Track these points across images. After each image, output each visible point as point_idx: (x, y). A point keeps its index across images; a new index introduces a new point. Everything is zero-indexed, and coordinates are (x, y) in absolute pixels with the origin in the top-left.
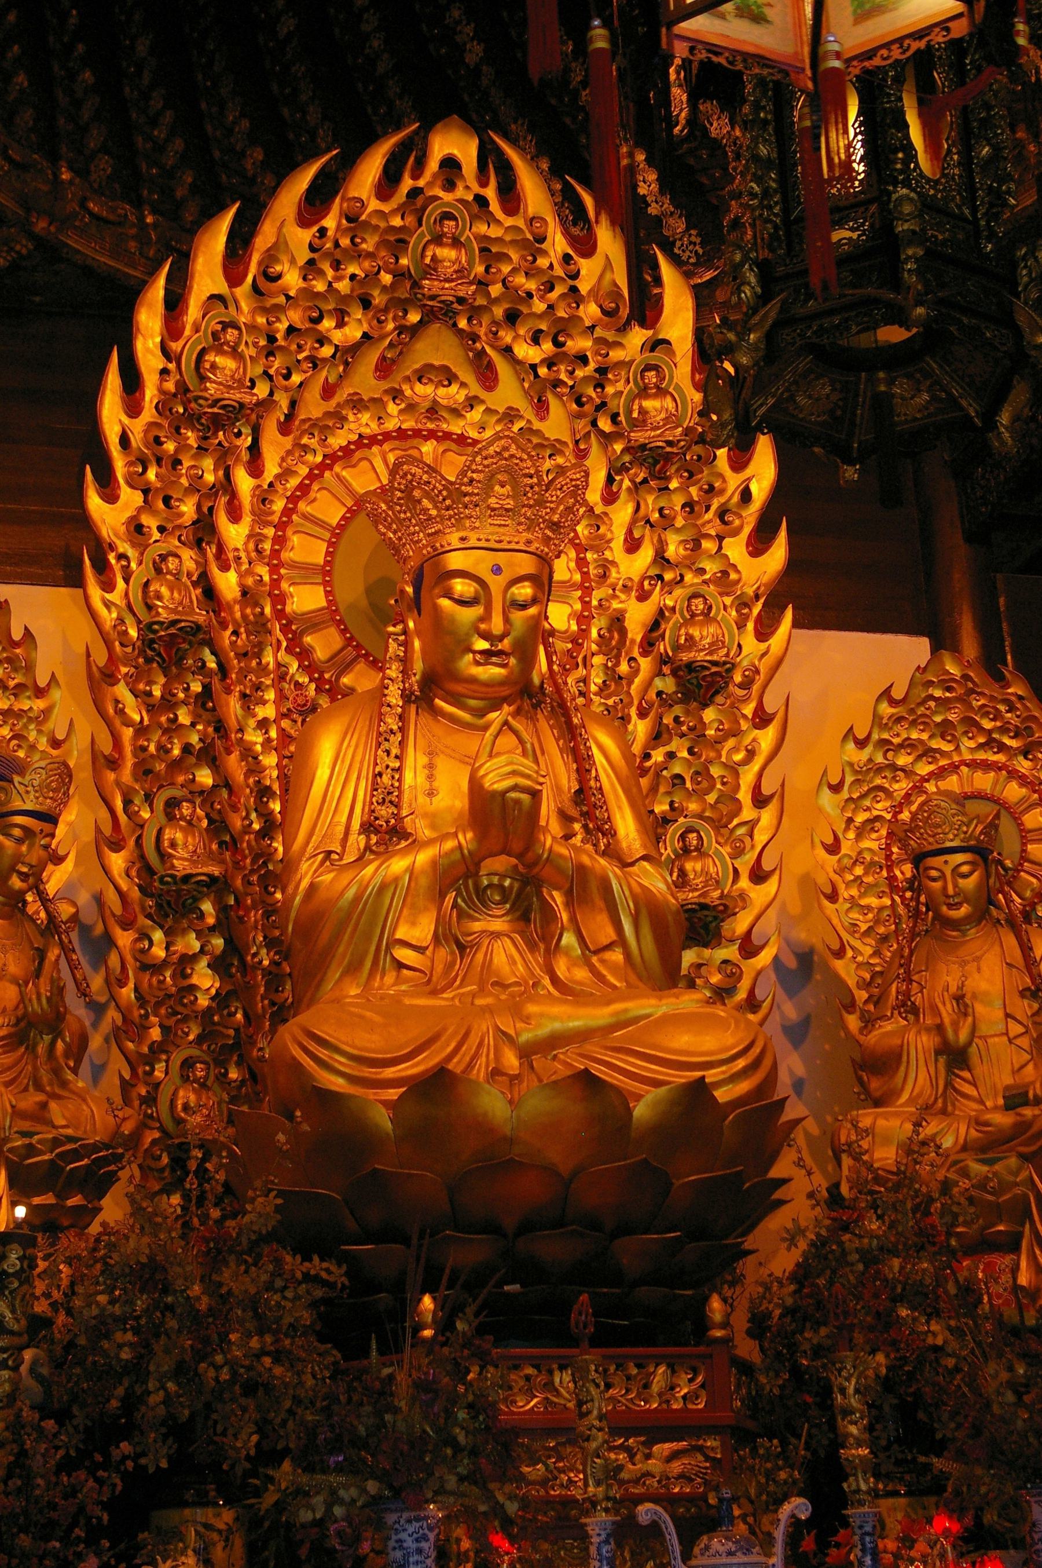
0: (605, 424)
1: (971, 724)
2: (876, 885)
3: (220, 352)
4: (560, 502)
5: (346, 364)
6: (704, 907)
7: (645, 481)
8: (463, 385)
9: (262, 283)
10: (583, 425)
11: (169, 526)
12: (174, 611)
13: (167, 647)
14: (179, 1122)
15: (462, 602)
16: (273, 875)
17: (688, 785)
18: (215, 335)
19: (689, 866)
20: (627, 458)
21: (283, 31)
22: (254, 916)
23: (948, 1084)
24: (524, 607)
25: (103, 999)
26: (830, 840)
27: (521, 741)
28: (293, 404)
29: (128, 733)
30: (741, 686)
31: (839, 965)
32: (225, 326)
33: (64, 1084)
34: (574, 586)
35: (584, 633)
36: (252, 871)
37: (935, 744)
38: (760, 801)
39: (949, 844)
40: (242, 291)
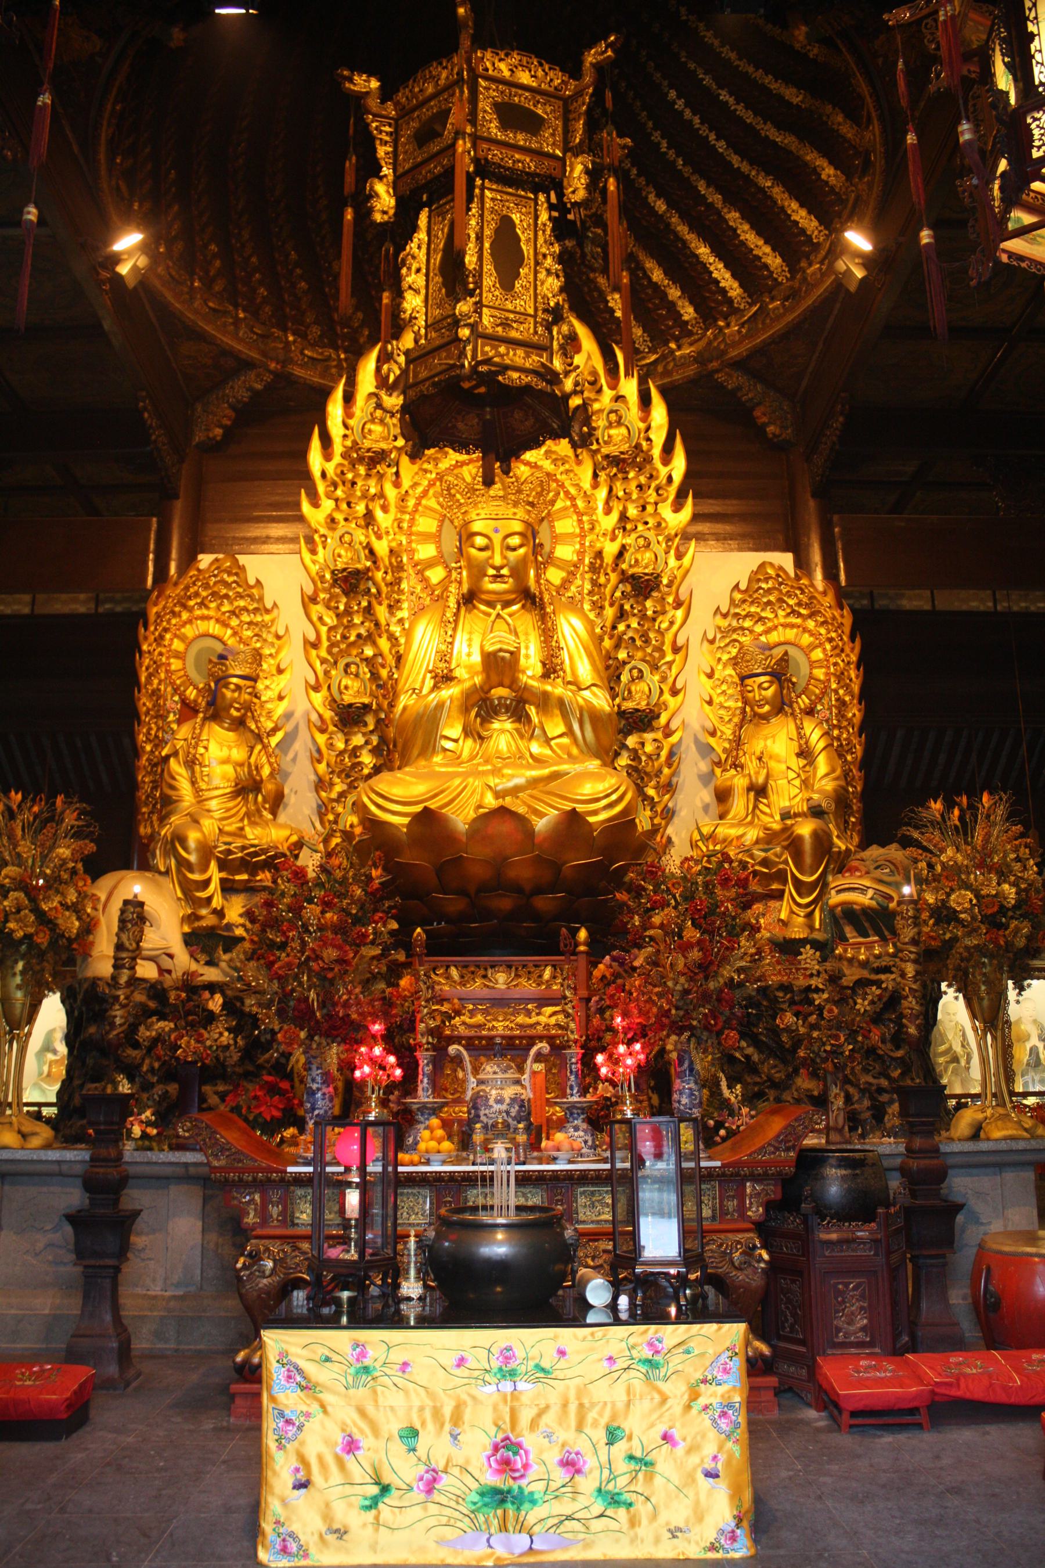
4: (531, 490)
6: (637, 710)
13: (350, 582)
15: (481, 549)
23: (755, 807)
24: (514, 549)
26: (709, 671)
29: (324, 630)
35: (581, 561)
37: (763, 614)
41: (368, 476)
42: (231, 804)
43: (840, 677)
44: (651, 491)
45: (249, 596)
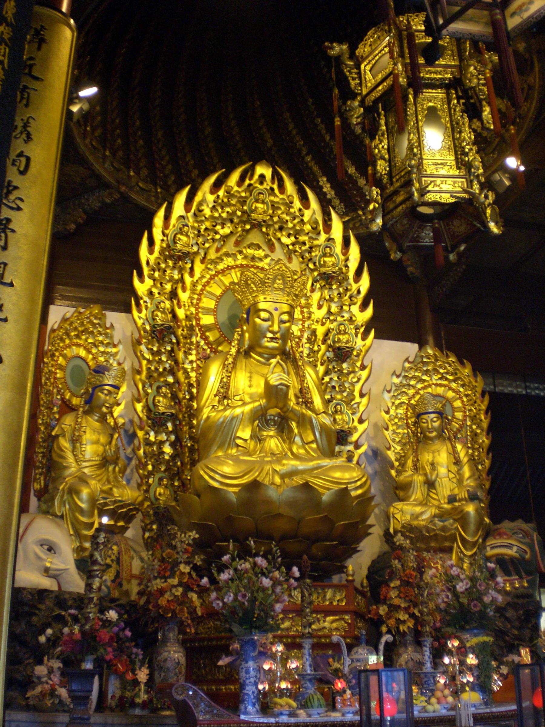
0: (311, 266)
1: (436, 371)
2: (402, 425)
3: (182, 234)
4: (299, 287)
5: (224, 241)
6: (342, 431)
7: (325, 285)
8: (264, 250)
9: (197, 213)
10: (304, 266)
11: (161, 293)
12: (163, 321)
13: (161, 333)
14: (157, 499)
15: (264, 320)
16: (193, 414)
17: (337, 389)
18: (181, 229)
19: (337, 417)
20: (318, 277)
21: (207, 132)
22: (186, 428)
23: (428, 495)
25: (131, 456)
27: (283, 369)
28: (205, 254)
30: (356, 356)
31: (389, 453)
32: (184, 226)
33: (118, 482)
34: (300, 320)
35: (302, 336)
36: (185, 413)
38: (362, 395)
39: (430, 411)
40: (190, 215)
41: (174, 268)
42: (98, 472)
43: (473, 418)
44: (346, 298)
45: (104, 334)
